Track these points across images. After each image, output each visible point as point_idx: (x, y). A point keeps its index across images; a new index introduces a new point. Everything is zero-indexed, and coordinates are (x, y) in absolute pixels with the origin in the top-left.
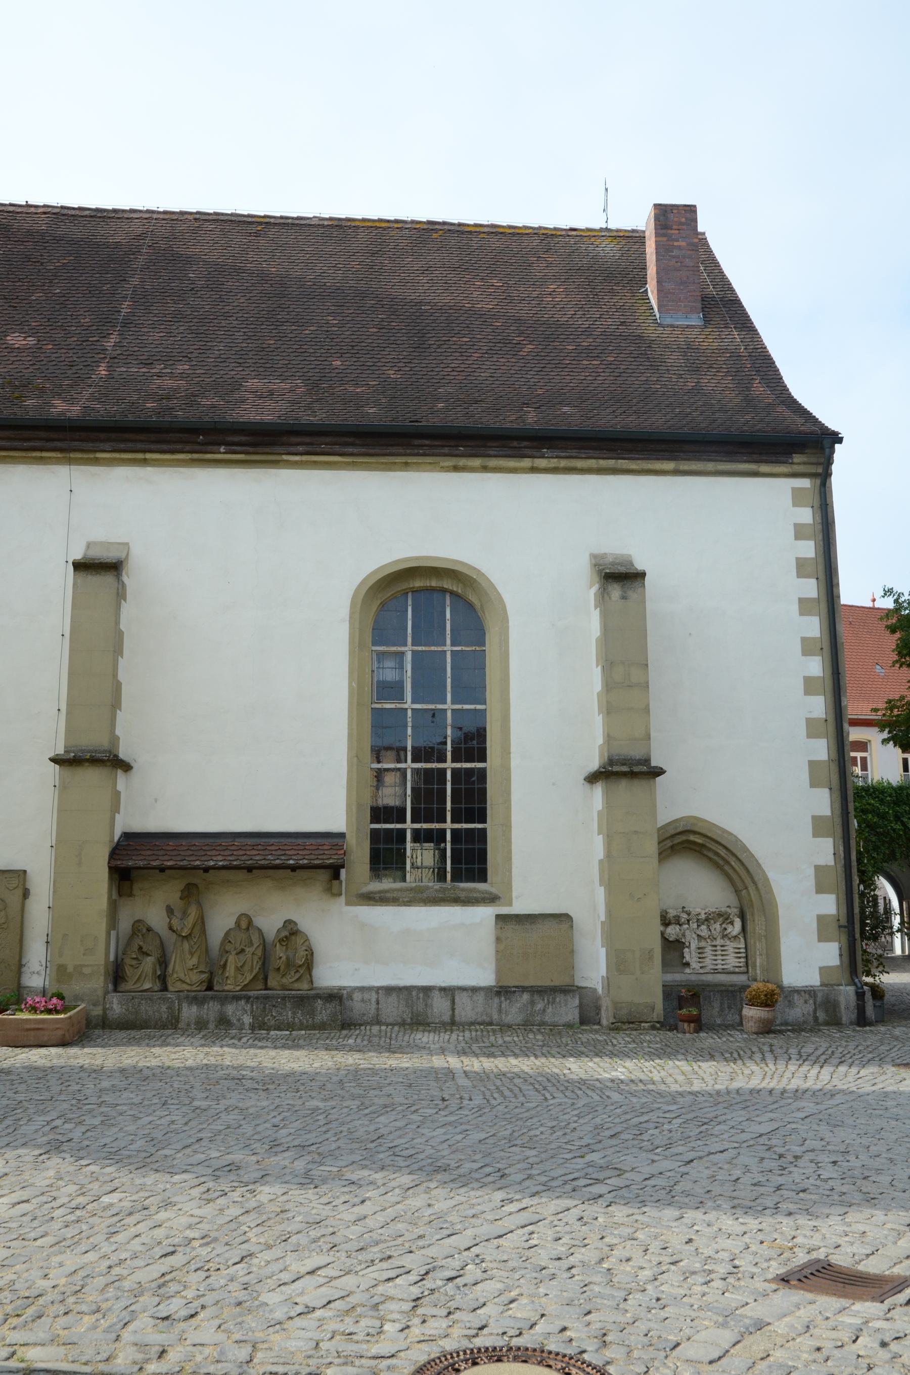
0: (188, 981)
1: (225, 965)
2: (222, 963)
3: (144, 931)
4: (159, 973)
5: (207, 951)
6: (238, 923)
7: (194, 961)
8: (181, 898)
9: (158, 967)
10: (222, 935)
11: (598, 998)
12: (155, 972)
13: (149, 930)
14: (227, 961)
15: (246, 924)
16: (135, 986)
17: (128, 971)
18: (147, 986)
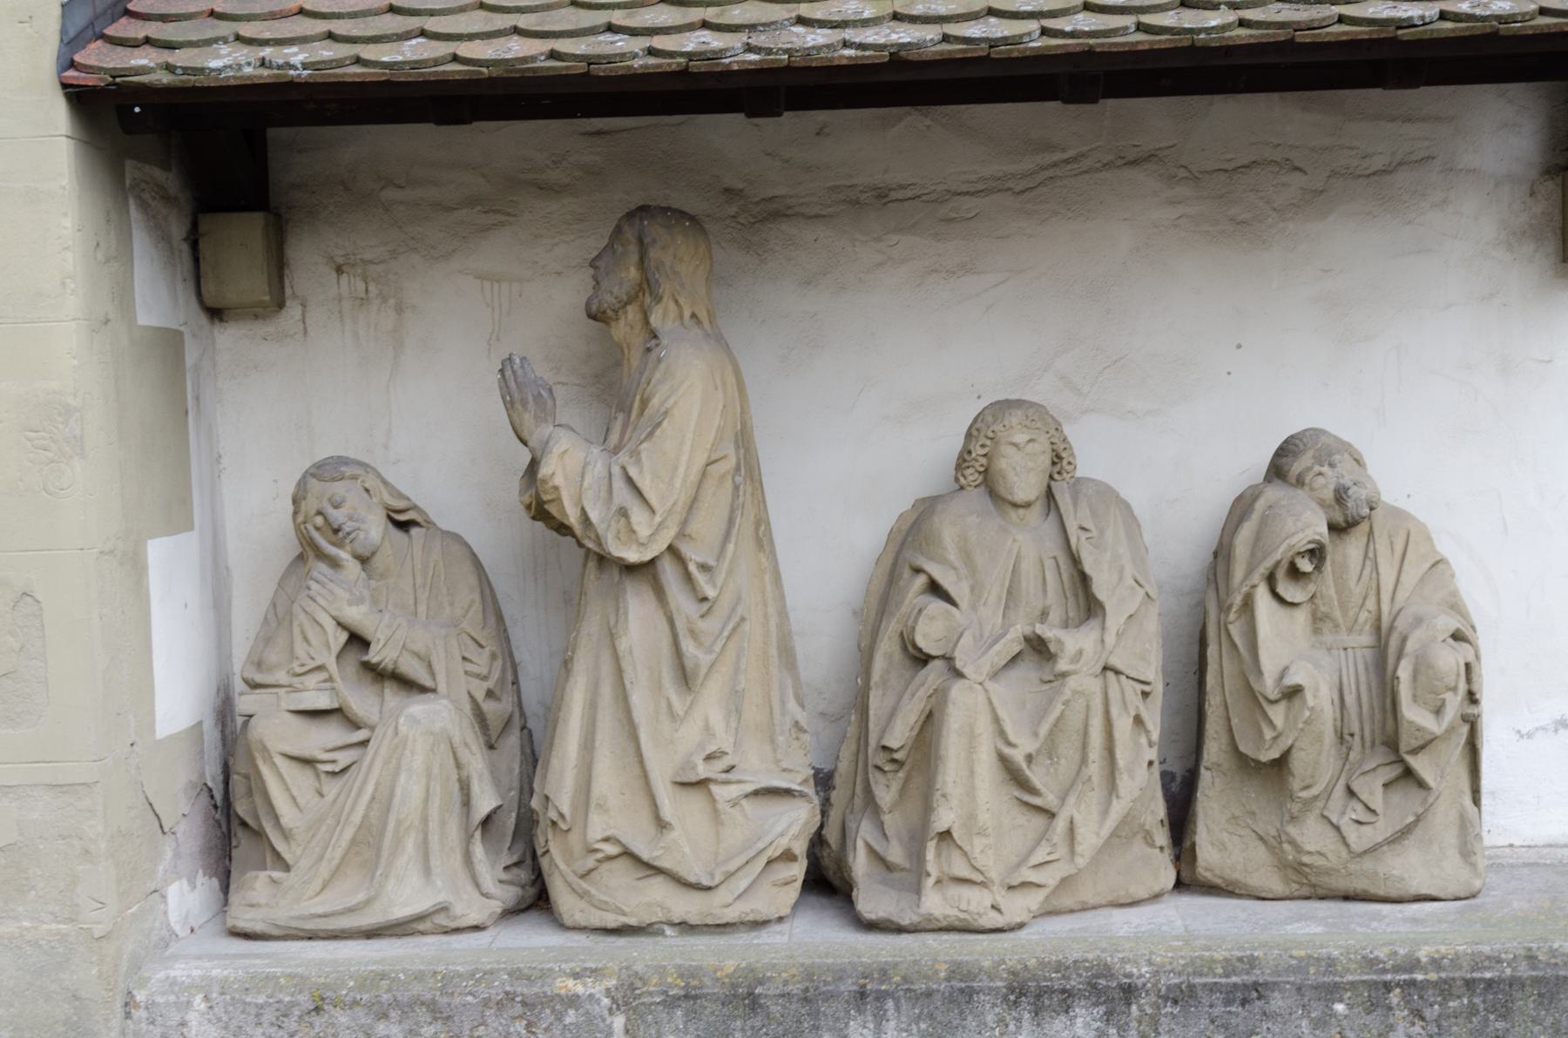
4: (485, 803)
14: (930, 721)
17: (289, 797)
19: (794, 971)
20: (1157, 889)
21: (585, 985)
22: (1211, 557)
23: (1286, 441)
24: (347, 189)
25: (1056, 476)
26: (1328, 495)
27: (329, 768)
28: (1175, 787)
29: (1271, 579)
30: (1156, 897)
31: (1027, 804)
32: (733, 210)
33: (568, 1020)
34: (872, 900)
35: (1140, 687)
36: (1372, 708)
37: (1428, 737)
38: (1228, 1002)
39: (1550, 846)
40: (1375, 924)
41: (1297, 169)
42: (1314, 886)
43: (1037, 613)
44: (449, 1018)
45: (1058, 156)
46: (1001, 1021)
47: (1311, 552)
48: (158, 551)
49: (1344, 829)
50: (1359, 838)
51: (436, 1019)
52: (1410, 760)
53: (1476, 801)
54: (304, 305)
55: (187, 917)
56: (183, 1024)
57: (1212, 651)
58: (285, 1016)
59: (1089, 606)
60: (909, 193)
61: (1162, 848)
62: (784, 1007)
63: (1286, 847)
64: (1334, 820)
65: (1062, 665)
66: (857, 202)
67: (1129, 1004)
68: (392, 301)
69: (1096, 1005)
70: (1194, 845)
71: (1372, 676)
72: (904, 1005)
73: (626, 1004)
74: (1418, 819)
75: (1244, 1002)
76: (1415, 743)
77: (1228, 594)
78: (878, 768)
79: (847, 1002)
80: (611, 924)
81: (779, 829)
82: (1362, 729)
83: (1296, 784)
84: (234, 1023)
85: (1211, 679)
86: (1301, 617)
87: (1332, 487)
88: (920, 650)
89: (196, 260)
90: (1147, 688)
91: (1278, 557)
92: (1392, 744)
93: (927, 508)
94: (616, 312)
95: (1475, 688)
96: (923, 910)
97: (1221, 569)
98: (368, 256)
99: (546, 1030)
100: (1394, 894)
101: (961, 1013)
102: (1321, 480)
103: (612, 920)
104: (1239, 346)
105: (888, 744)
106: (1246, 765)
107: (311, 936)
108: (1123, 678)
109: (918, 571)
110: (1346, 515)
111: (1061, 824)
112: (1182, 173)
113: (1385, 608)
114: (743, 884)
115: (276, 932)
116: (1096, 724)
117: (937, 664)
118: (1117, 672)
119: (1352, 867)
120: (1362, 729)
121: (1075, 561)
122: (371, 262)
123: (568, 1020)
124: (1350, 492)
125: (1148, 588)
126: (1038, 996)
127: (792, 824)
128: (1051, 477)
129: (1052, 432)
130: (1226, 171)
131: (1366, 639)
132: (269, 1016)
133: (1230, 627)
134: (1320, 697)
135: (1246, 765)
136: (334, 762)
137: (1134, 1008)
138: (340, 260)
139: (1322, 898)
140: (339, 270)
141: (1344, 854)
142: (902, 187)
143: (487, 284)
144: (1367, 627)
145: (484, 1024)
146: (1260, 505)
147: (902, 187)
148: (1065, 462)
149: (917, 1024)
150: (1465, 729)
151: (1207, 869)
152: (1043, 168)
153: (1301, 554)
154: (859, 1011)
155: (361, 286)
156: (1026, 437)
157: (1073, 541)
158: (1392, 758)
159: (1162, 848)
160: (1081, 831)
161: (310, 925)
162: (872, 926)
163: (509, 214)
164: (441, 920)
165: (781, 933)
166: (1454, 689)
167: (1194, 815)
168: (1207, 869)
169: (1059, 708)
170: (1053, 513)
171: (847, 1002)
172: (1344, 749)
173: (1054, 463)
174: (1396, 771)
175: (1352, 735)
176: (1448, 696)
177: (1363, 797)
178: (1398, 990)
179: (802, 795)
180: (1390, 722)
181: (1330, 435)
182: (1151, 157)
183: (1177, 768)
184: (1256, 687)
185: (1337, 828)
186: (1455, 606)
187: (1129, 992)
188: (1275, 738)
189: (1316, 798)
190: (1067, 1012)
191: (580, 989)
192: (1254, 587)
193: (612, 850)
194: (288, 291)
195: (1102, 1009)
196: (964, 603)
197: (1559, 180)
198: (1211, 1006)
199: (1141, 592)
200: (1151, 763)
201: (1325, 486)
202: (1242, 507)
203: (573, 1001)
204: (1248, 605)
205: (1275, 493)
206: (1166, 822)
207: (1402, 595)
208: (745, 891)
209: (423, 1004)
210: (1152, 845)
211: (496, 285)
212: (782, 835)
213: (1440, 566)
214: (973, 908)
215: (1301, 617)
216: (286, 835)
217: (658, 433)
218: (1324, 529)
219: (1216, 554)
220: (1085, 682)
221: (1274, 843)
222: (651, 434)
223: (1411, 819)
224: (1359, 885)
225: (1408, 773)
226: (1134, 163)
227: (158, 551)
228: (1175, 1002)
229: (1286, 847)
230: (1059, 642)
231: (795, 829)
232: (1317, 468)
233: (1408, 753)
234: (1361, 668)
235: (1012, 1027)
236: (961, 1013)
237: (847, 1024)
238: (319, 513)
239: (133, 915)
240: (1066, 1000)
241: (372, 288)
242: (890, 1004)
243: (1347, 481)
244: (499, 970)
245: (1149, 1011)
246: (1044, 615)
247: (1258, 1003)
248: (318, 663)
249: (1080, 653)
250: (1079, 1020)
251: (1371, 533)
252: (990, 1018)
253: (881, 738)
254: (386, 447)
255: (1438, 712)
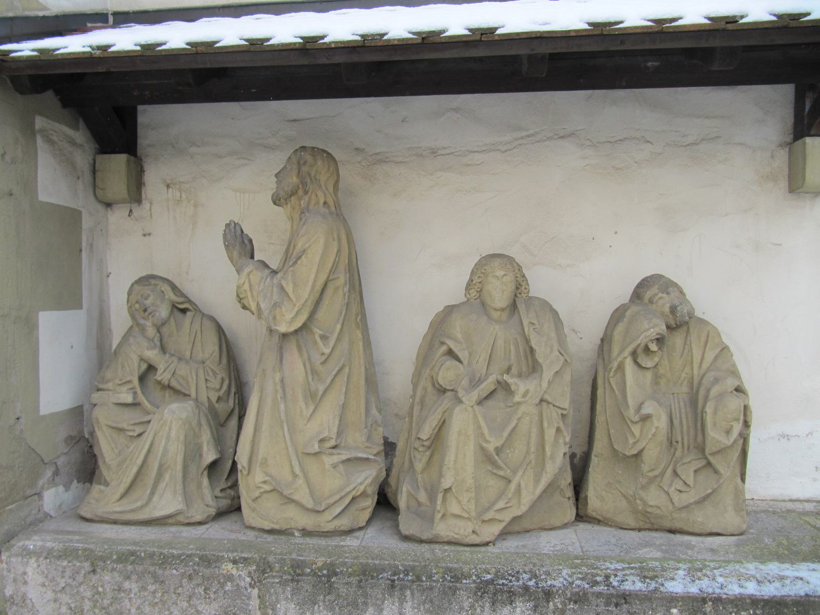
0: (302, 495)
1: (438, 439)
2: (426, 432)
3: (163, 312)
4: (210, 456)
5: (372, 382)
6: (476, 283)
7: (325, 421)
8: (277, 201)
9: (206, 437)
10: (421, 326)
11: (90, 52)
12: (192, 452)
13: (183, 308)
14: (443, 425)
15: (504, 295)
16: (125, 505)
17: (106, 447)
18: (167, 503)
19: (355, 568)
20: (566, 521)
21: (238, 569)
22: (599, 342)
23: (643, 280)
24: (173, 147)
25: (518, 295)
26: (667, 309)
27: (131, 434)
28: (576, 461)
29: (634, 354)
30: (565, 526)
31: (495, 474)
32: (359, 159)
33: (227, 588)
34: (407, 524)
35: (560, 411)
36: (688, 427)
37: (723, 446)
38: (607, 604)
39: (774, 500)
40: (690, 552)
41: (648, 142)
42: (653, 524)
43: (506, 368)
44: (162, 582)
45: (524, 134)
46: (472, 607)
47: (658, 339)
48: (47, 320)
49: (671, 494)
50: (681, 500)
51: (156, 582)
52: (711, 458)
53: (743, 480)
54: (151, 203)
55: (60, 506)
56: (25, 573)
57: (600, 392)
58: (77, 573)
59: (533, 367)
60: (448, 151)
61: (569, 498)
62: (347, 589)
63: (638, 501)
64: (666, 489)
65: (517, 398)
66: (422, 155)
67: (548, 602)
68: (192, 202)
69: (529, 601)
70: (586, 497)
71: (689, 409)
72: (417, 594)
73: (260, 581)
74: (714, 491)
75: (617, 605)
76: (714, 449)
77: (610, 362)
78: (415, 449)
79: (384, 589)
80: (267, 528)
81: (359, 481)
82: (683, 439)
83: (645, 468)
84: (50, 576)
85: (599, 407)
86: (649, 375)
87: (668, 305)
88: (441, 386)
89: (94, 178)
90: (565, 412)
91: (639, 342)
92: (701, 449)
93: (450, 310)
94: (286, 200)
95: (748, 420)
96: (434, 532)
97: (606, 348)
98: (182, 180)
99: (215, 593)
100: (697, 531)
101: (449, 600)
102: (661, 302)
103: (267, 525)
104: (616, 233)
105: (420, 437)
106: (617, 457)
107: (115, 522)
108: (551, 406)
109: (443, 343)
110: (676, 321)
111: (513, 486)
112: (588, 143)
113: (696, 372)
114: (338, 510)
115: (97, 519)
116: (535, 431)
117: (449, 394)
118: (548, 403)
119: (675, 515)
120: (683, 439)
121: (527, 341)
122: (183, 183)
123: (227, 588)
124: (679, 308)
125: (566, 357)
126: (495, 594)
127: (365, 479)
128: (516, 295)
129: (517, 271)
130: (610, 142)
131: (685, 389)
132: (68, 573)
133: (611, 379)
134: (661, 423)
135: (617, 457)
136: (134, 431)
137: (551, 603)
138: (169, 182)
139: (657, 530)
140: (168, 186)
141: (671, 507)
142: (444, 148)
143: (238, 194)
144: (685, 382)
145: (181, 586)
146: (628, 313)
147: (444, 148)
148: (523, 288)
149: (424, 604)
150: (741, 441)
151: (593, 511)
152: (516, 139)
153: (652, 341)
154: (391, 596)
155: (178, 194)
156: (503, 273)
157: (526, 330)
158: (700, 456)
159: (569, 498)
160: (524, 492)
161: (114, 517)
162: (406, 538)
163: (249, 160)
164: (181, 518)
165: (357, 538)
166: (737, 420)
167: (587, 480)
168: (593, 511)
169: (515, 422)
170: (516, 317)
171: (384, 589)
172: (673, 450)
173: (517, 288)
174: (704, 462)
175: (677, 442)
176: (734, 424)
177: (683, 477)
178: (710, 603)
179: (375, 461)
180: (700, 437)
181: (412, 379)
182: (572, 135)
183: (579, 452)
184: (625, 414)
185: (667, 493)
186: (735, 373)
187: (548, 594)
188: (635, 443)
189: (656, 477)
190: (511, 604)
191: (234, 572)
192: (625, 358)
193: (267, 487)
194: (143, 196)
195: (532, 604)
196: (465, 362)
197: (787, 149)
198: (597, 606)
199: (562, 359)
200: (565, 454)
201: (663, 305)
202: (618, 315)
203: (230, 578)
204: (621, 367)
205: (634, 309)
206: (572, 484)
207: (705, 366)
208: (340, 514)
209: (149, 573)
210: (564, 497)
211: (242, 195)
212: (361, 484)
213: (726, 350)
214: (462, 532)
215: (649, 375)
216: (109, 468)
217: (299, 262)
218: (664, 328)
219: (602, 340)
220: (528, 409)
221: (631, 499)
222: (295, 262)
223: (710, 491)
224: (677, 525)
225: (709, 464)
226: (562, 137)
227: (47, 320)
228: (575, 602)
229: (638, 501)
230: (516, 384)
231: (369, 481)
232: (660, 295)
233: (711, 454)
234: (682, 404)
235: (478, 610)
236: (449, 600)
237: (383, 602)
238: (137, 302)
239: (11, 510)
240: (511, 596)
241: (183, 195)
242: (408, 593)
243: (676, 302)
244: (195, 555)
245: (560, 606)
246: (508, 371)
247: (625, 606)
248: (128, 379)
249: (527, 392)
250: (518, 609)
251: (688, 328)
252: (466, 605)
253: (417, 433)
254: (187, 273)
255: (728, 432)
